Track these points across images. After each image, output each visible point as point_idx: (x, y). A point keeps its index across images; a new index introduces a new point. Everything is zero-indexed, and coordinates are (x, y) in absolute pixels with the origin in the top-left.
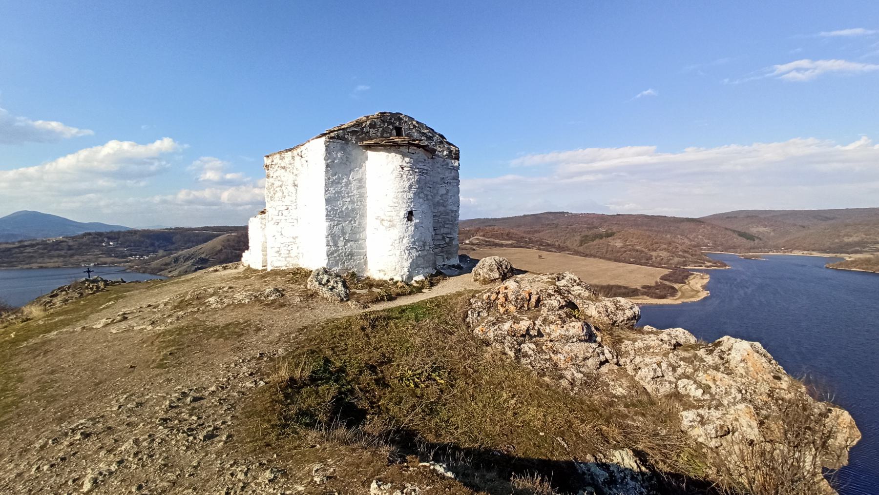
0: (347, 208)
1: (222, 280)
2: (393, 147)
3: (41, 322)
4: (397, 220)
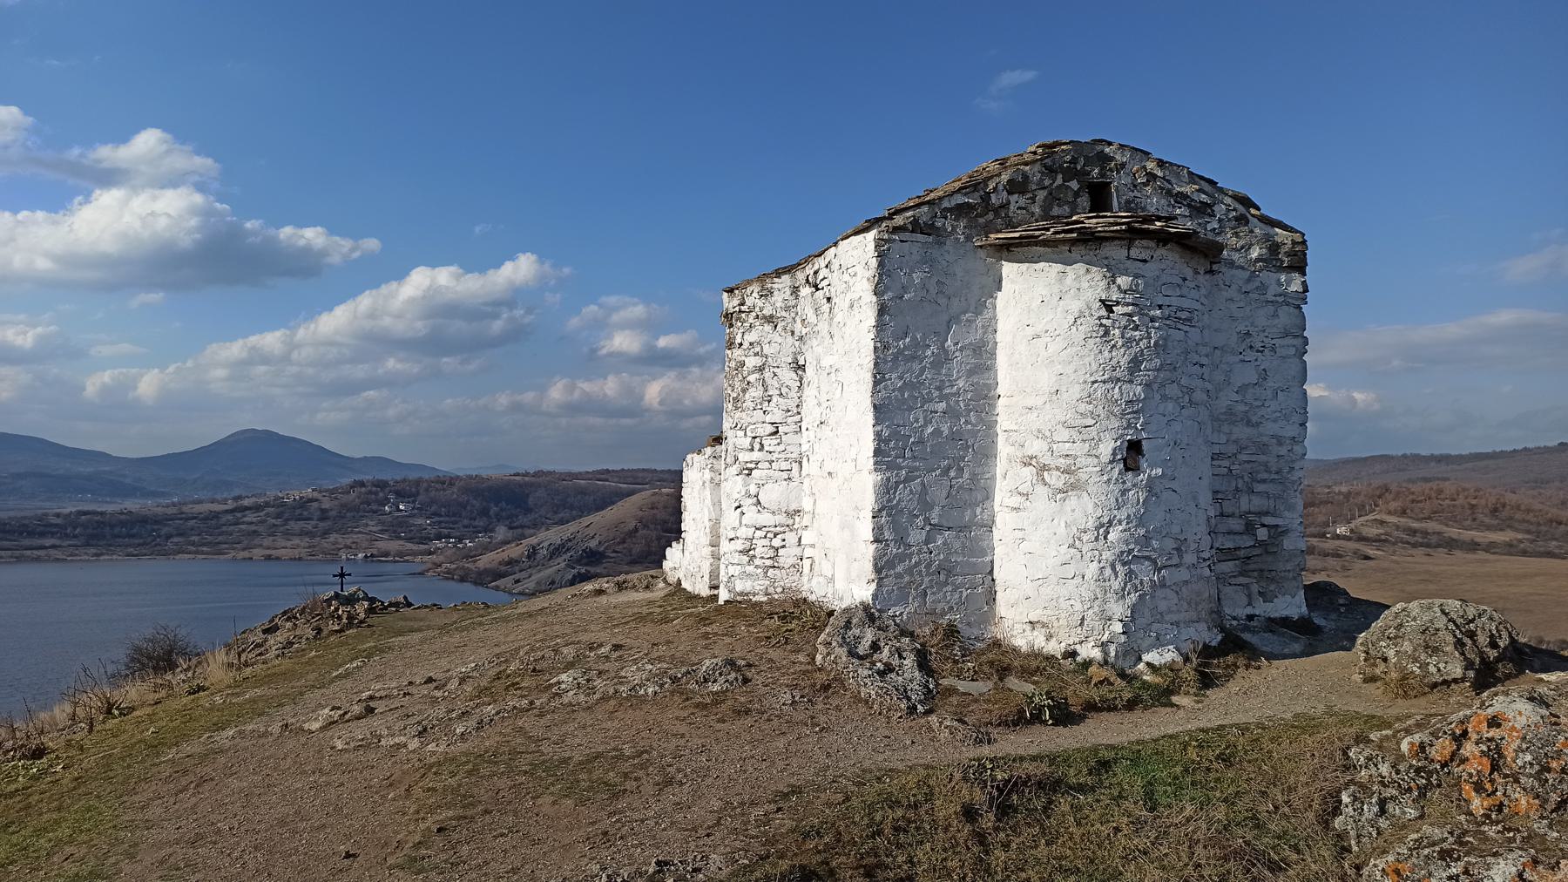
0: (937, 432)
1: (610, 621)
2: (1085, 244)
3: (218, 699)
4: (1089, 470)
